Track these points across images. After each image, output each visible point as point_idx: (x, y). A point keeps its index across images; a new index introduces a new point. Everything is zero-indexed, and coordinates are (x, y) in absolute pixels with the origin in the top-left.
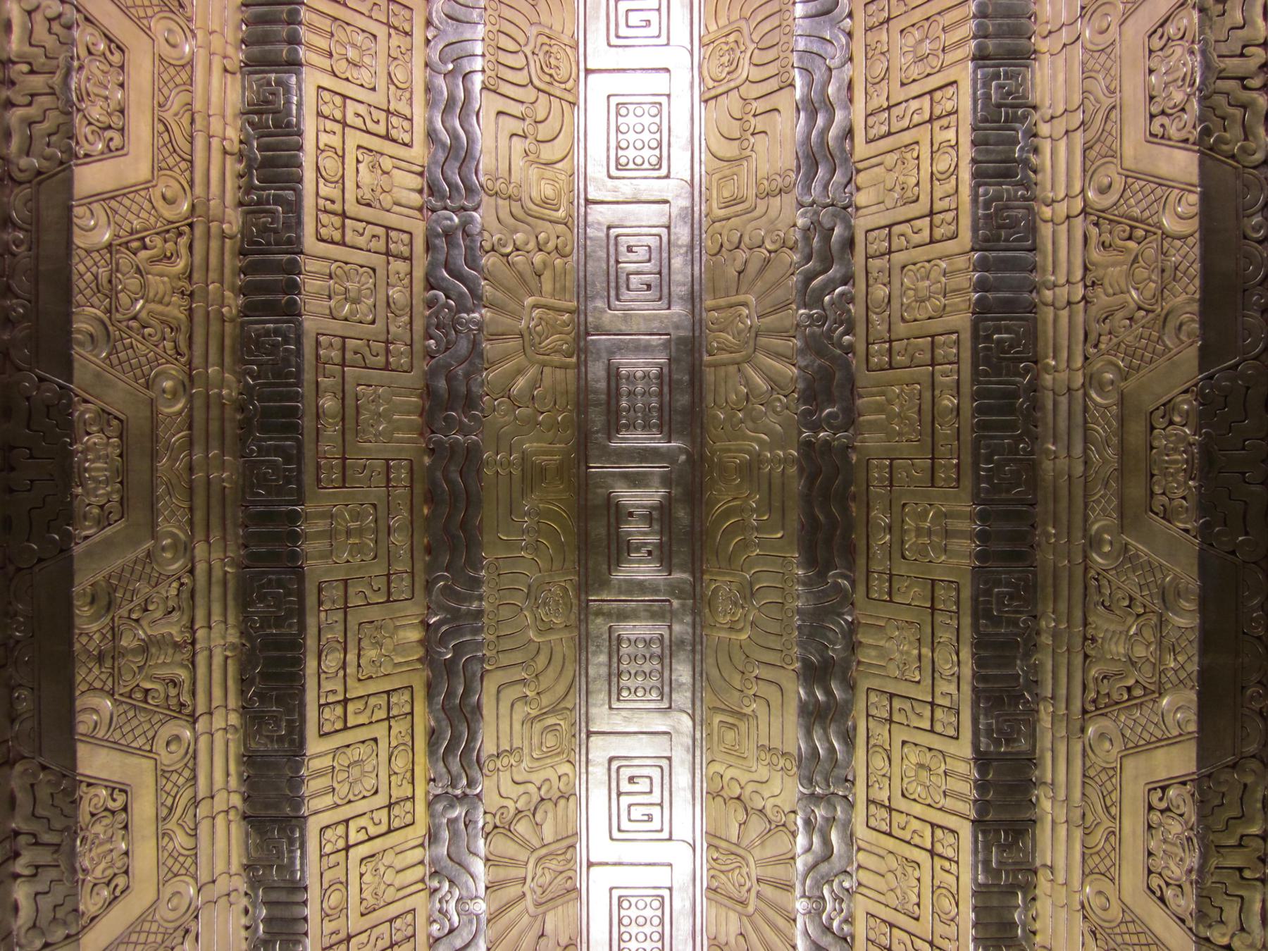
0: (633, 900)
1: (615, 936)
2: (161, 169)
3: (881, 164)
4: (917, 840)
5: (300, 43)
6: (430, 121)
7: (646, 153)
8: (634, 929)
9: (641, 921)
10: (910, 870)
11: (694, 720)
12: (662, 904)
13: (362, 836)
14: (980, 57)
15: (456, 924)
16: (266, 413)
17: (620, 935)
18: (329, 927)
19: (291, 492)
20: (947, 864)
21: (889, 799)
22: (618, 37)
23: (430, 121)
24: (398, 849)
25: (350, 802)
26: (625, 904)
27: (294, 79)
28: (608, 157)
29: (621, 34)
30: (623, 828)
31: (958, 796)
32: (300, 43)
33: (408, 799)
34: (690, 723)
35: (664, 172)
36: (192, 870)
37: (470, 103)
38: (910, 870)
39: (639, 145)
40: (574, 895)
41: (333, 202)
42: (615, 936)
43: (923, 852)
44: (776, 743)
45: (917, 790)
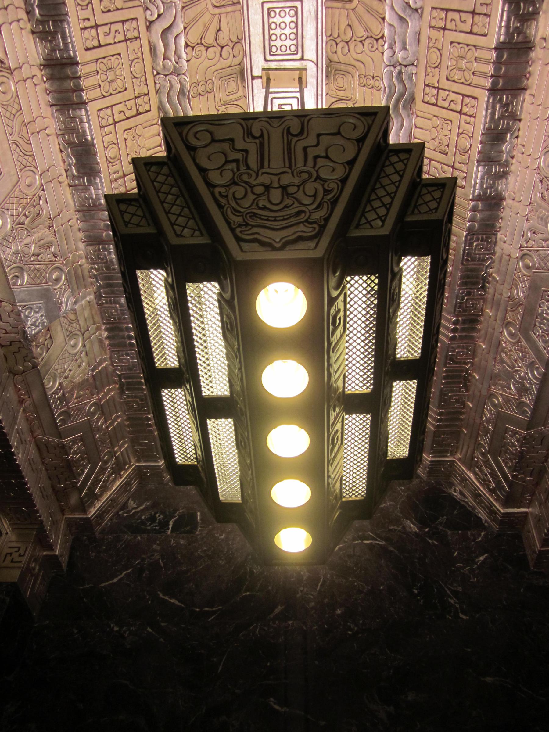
0: (278, 11)
1: (267, 37)
2: (21, 170)
3: (430, 120)
4: (453, 106)
5: (82, 90)
6: (160, 102)
7: (288, 43)
8: (278, 32)
9: (283, 25)
10: (445, 125)
11: (317, 66)
12: (296, 13)
13: (122, 117)
14: (493, 91)
15: (162, 11)
16: (128, 384)
17: (270, 37)
18: (112, 169)
19: (145, 410)
20: (468, 119)
21: (438, 82)
22: (271, 55)
23: (160, 102)
24: (144, 125)
25: (111, 94)
26: (273, 14)
27: (83, 112)
28: (269, 147)
29: (274, 101)
30: (274, 101)
31: (483, 75)
32: (82, 90)
33: (145, 95)
34: (315, 69)
35: (299, 56)
36: (34, 163)
37: (175, 26)
38: (445, 125)
39: (283, 37)
40: (238, 7)
41: (88, 19)
42: (267, 37)
43: (456, 113)
44: (369, 91)
45: (457, 75)
